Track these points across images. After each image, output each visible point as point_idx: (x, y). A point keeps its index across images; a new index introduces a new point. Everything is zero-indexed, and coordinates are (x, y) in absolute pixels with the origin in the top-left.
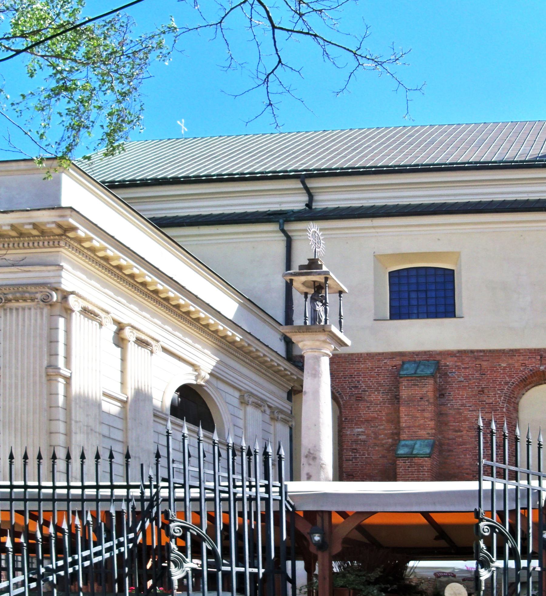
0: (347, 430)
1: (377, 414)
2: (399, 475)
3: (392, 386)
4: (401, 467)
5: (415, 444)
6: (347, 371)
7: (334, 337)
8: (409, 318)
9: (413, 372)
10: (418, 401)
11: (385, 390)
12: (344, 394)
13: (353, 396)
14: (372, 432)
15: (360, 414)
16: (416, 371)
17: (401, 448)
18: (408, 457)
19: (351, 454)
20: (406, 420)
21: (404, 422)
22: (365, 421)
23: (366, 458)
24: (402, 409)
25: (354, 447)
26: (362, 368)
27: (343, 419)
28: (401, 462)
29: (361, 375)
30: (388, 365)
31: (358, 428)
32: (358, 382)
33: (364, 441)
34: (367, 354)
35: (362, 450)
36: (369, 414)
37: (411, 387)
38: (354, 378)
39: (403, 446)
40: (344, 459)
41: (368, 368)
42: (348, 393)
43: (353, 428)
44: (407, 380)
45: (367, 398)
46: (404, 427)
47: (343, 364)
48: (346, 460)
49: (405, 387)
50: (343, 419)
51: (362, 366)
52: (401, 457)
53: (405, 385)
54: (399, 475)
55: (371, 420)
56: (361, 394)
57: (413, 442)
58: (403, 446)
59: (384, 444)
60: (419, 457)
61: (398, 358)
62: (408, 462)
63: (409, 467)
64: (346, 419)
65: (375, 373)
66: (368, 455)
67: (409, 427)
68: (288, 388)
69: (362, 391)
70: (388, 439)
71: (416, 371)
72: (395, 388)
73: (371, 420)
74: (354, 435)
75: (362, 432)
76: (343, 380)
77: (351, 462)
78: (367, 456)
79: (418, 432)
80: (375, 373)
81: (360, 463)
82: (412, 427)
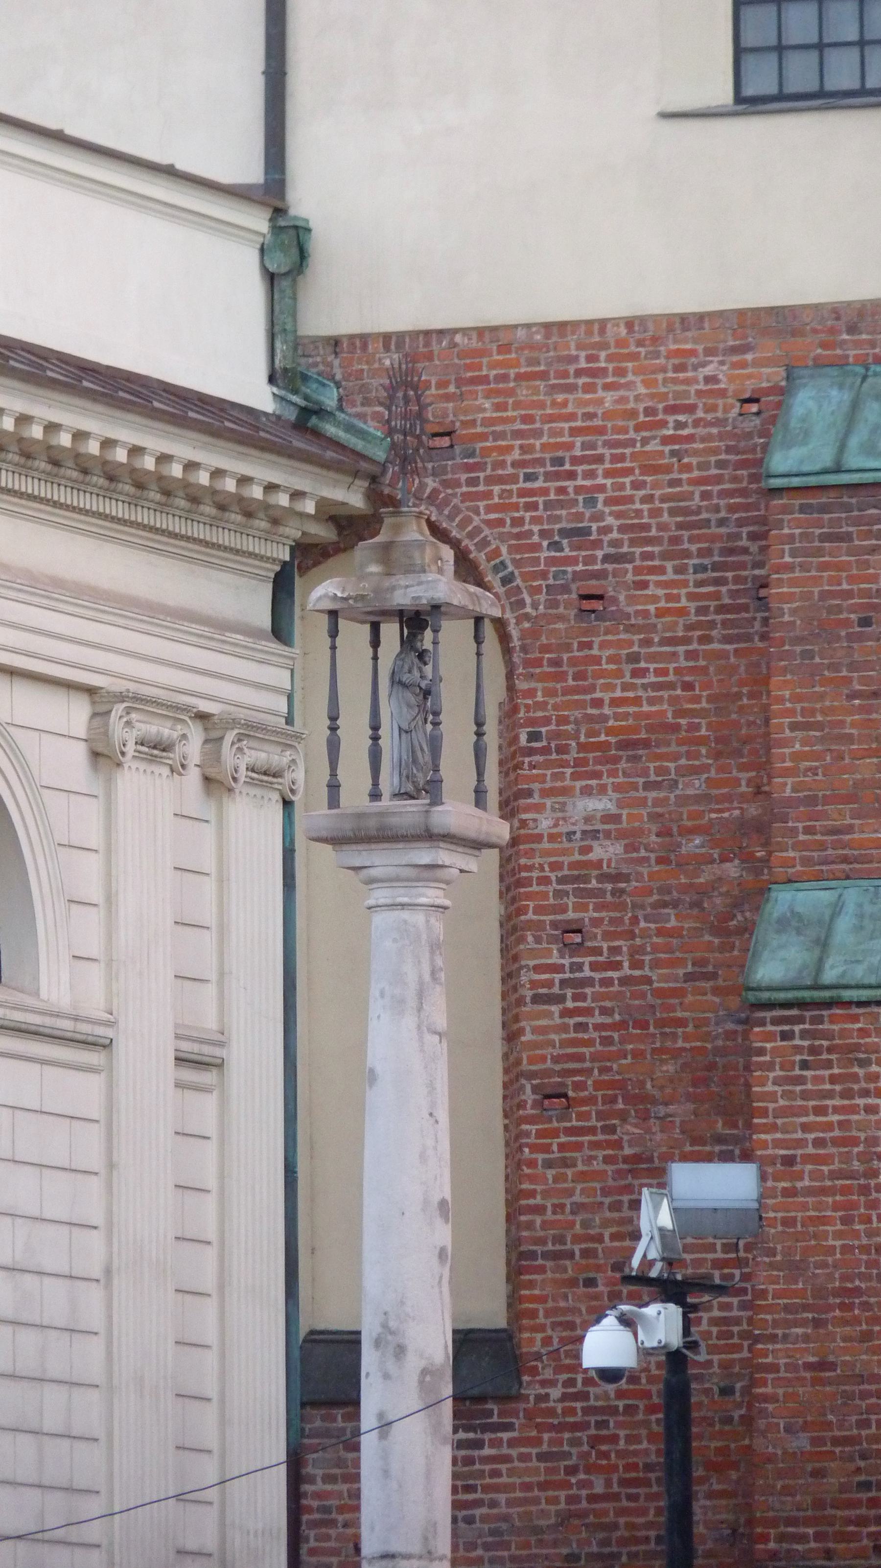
0: (539, 808)
1: (673, 701)
2: (764, 1113)
3: (740, 523)
4: (770, 1066)
5: (837, 909)
6: (538, 434)
7: (288, 832)
8: (741, 313)
9: (826, 459)
10: (850, 637)
11: (708, 552)
12: (525, 577)
13: (565, 589)
14: (655, 817)
15: (598, 703)
16: (842, 448)
17: (775, 940)
18: (802, 1005)
19: (555, 959)
20: (797, 757)
21: (787, 773)
22: (624, 745)
23: (625, 981)
24: (783, 688)
25: (571, 915)
26: (607, 415)
27: (523, 739)
28: (769, 1037)
29: (600, 459)
30: (723, 393)
31: (587, 792)
32: (591, 502)
33: (619, 877)
34: (630, 323)
35: (608, 936)
36: (637, 701)
37: (819, 552)
38: (572, 475)
39: (783, 924)
40: (528, 994)
41: (633, 414)
42: (544, 575)
43: (565, 791)
44: (803, 509)
45: (632, 600)
46: (790, 802)
47: (523, 393)
48: (536, 999)
49: (794, 553)
50: (523, 739)
51: (609, 398)
52: (770, 1005)
53: (791, 538)
54: (764, 1113)
55: (646, 744)
56: (601, 575)
57: (826, 897)
58: (783, 924)
59: (704, 891)
60: (849, 1004)
61: (770, 348)
62: (804, 1034)
63: (805, 1065)
64: (534, 737)
65: (666, 440)
66: (636, 964)
67: (812, 800)
68: (272, 570)
69: (607, 558)
70: (724, 859)
71: (842, 448)
72: (753, 537)
73: (646, 744)
74: (570, 835)
75: (609, 818)
76: (522, 493)
77: (555, 1009)
78: (626, 970)
79: (850, 829)
80: (666, 440)
81: (598, 1019)
82: (827, 800)
